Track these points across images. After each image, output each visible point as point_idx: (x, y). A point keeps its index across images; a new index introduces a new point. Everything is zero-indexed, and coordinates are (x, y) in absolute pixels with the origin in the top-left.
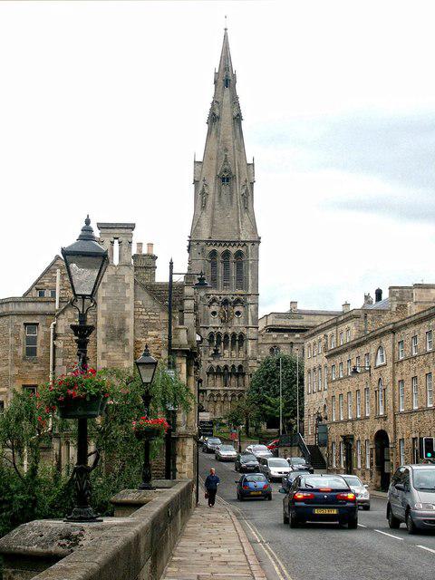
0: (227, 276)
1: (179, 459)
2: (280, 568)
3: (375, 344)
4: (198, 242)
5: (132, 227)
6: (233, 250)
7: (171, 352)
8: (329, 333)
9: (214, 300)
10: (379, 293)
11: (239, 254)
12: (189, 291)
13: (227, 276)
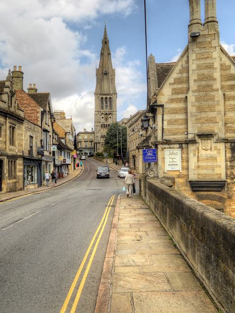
6: (108, 97)
9: (102, 113)
11: (110, 98)
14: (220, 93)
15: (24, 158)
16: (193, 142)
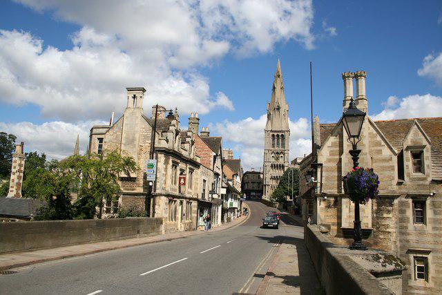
0: (278, 144)
6: (280, 134)
11: (282, 135)
13: (278, 144)
15: (167, 196)
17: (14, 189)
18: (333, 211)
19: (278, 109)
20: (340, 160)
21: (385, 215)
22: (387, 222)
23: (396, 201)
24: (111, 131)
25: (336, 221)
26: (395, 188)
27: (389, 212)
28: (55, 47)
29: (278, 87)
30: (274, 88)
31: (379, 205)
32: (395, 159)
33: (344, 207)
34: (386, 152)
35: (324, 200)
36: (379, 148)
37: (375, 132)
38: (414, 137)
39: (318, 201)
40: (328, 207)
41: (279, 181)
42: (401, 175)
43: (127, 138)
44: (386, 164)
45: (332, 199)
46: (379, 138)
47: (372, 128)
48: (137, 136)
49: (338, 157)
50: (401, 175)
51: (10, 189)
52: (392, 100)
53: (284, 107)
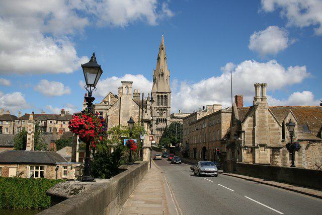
0: (162, 103)
1: (144, 155)
2: (172, 195)
3: (203, 121)
4: (154, 92)
5: (132, 83)
6: (164, 95)
7: (142, 122)
8: (190, 118)
9: (158, 109)
10: (204, 107)
11: (165, 96)
12: (148, 103)
13: (162, 103)
14: (268, 128)
15: (149, 148)
16: (257, 147)
17: (30, 145)
18: (250, 155)
19: (163, 75)
20: (254, 129)
21: (276, 157)
22: (277, 160)
23: (281, 150)
24: (112, 108)
25: (252, 160)
26: (281, 143)
27: (278, 155)
28: (128, 74)
29: (162, 57)
30: (159, 58)
31: (273, 152)
32: (281, 129)
33: (256, 153)
34: (277, 125)
35: (246, 150)
36: (273, 123)
37: (271, 115)
38: (290, 117)
39: (243, 150)
40: (248, 153)
41: (163, 132)
42: (284, 137)
43: (124, 113)
44: (276, 131)
45: (250, 149)
46: (273, 119)
47: (269, 113)
48: (130, 112)
49: (252, 127)
50: (284, 137)
51: (27, 145)
52: (229, 66)
53: (167, 73)
